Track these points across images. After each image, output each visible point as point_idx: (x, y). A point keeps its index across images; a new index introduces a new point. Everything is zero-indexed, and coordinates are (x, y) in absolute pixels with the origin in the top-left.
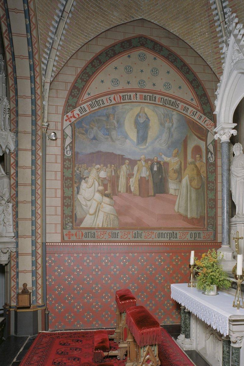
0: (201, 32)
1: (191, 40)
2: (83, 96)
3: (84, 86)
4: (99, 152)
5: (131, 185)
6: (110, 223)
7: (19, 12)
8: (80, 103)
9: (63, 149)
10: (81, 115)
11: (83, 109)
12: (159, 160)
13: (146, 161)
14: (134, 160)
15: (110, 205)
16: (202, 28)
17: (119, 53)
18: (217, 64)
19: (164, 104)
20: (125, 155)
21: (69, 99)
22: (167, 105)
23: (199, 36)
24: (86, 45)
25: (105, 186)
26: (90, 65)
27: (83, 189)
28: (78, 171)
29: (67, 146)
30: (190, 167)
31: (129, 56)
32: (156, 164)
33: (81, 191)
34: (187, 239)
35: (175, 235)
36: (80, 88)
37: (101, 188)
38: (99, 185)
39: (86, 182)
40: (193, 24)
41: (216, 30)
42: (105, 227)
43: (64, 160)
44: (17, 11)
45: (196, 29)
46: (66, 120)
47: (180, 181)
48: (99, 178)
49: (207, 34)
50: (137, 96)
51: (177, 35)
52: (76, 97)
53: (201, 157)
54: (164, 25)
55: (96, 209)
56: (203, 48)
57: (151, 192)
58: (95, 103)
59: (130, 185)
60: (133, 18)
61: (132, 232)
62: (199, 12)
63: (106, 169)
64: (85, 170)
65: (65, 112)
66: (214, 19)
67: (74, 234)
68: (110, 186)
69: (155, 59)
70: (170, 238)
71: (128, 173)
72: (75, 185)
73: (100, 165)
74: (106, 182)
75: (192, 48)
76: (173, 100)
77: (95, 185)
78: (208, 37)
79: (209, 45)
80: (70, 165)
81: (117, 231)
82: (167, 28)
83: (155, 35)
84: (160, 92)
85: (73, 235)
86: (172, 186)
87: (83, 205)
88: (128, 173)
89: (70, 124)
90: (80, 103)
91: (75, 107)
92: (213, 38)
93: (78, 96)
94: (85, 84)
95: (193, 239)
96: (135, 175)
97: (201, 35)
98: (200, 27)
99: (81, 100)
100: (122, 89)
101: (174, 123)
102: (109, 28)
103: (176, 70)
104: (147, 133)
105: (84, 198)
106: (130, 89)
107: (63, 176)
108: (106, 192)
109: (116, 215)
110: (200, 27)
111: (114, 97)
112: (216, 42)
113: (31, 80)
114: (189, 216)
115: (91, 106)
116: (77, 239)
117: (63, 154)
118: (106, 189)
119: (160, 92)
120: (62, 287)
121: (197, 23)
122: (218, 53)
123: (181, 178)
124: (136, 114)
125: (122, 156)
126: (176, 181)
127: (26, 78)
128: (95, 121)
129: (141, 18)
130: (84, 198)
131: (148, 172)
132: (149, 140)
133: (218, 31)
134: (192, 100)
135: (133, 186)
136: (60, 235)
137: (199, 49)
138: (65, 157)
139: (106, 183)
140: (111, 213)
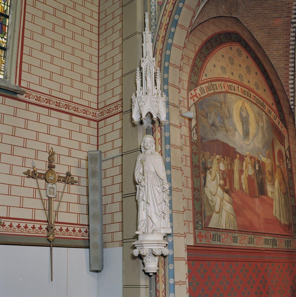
0: (277, 48)
1: (269, 50)
2: (202, 75)
3: (202, 66)
4: (217, 140)
5: (243, 183)
6: (231, 224)
7: (175, 189)
8: (200, 82)
9: (191, 130)
10: (202, 96)
11: (202, 90)
12: (259, 159)
13: (251, 158)
14: (243, 155)
15: (229, 203)
16: (279, 46)
17: (224, 42)
18: (285, 78)
19: (256, 102)
20: (236, 148)
21: (191, 76)
22: (258, 105)
23: (275, 50)
24: (201, 25)
25: (224, 180)
26: (205, 46)
27: (208, 181)
28: (203, 159)
29: (193, 128)
30: (278, 170)
31: (231, 48)
32: (257, 162)
33: (208, 184)
34: (283, 247)
35: (275, 242)
36: (199, 67)
37: (222, 182)
38: (220, 179)
39: (211, 173)
40: (273, 39)
41: (289, 51)
42: (228, 228)
43: (192, 143)
44: (176, 190)
45: (274, 44)
46: (191, 98)
47: (274, 184)
48: (220, 170)
49: (281, 51)
50: (239, 88)
51: (259, 42)
52: (197, 75)
53: (283, 161)
54: (251, 30)
55: (220, 206)
56: (276, 61)
57: (257, 194)
58: (211, 86)
59: (242, 183)
60: (231, 14)
61: (247, 236)
62: (280, 33)
63: (224, 161)
64: (209, 159)
65: (189, 90)
66: (290, 43)
67: (204, 235)
68: (228, 181)
69: (247, 57)
70: (273, 245)
71: (239, 168)
72: (202, 175)
73: (219, 155)
74: (225, 176)
75: (268, 57)
76: (262, 101)
77: (217, 178)
78: (281, 54)
79: (281, 61)
80: (197, 150)
81: (236, 235)
82: (253, 33)
83: (245, 36)
84: (252, 89)
85: (203, 236)
86: (269, 188)
87: (210, 200)
88: (239, 168)
89: (194, 104)
90: (200, 82)
91: (196, 86)
92: (286, 56)
93: (198, 74)
94: (203, 64)
95: (286, 247)
96: (244, 172)
97: (277, 50)
98: (278, 43)
99: (200, 80)
100: (228, 78)
101: (265, 123)
102: (215, 16)
103: (225, 45)
104: (249, 127)
105: (210, 192)
106: (233, 80)
107: (192, 162)
108: (226, 187)
109: (235, 215)
110: (278, 43)
111: (224, 84)
112: (287, 60)
113: (168, 82)
114: (282, 222)
115: (208, 89)
116: (207, 242)
117: (191, 138)
118: (225, 184)
119: (252, 89)
120: (196, 288)
121: (276, 39)
122: (287, 69)
123: (274, 181)
124: (240, 107)
125: (235, 149)
126: (271, 183)
127: (181, 259)
128: (212, 105)
129: (235, 16)
130: (210, 192)
131: (253, 171)
132: (251, 136)
133: (291, 53)
134: (272, 104)
135: (244, 184)
136: (192, 235)
137: (273, 61)
138: (192, 141)
139: (225, 177)
140: (231, 213)
